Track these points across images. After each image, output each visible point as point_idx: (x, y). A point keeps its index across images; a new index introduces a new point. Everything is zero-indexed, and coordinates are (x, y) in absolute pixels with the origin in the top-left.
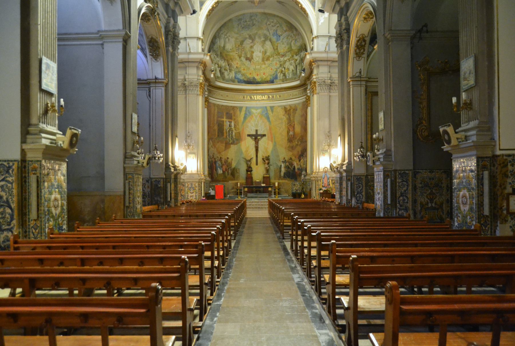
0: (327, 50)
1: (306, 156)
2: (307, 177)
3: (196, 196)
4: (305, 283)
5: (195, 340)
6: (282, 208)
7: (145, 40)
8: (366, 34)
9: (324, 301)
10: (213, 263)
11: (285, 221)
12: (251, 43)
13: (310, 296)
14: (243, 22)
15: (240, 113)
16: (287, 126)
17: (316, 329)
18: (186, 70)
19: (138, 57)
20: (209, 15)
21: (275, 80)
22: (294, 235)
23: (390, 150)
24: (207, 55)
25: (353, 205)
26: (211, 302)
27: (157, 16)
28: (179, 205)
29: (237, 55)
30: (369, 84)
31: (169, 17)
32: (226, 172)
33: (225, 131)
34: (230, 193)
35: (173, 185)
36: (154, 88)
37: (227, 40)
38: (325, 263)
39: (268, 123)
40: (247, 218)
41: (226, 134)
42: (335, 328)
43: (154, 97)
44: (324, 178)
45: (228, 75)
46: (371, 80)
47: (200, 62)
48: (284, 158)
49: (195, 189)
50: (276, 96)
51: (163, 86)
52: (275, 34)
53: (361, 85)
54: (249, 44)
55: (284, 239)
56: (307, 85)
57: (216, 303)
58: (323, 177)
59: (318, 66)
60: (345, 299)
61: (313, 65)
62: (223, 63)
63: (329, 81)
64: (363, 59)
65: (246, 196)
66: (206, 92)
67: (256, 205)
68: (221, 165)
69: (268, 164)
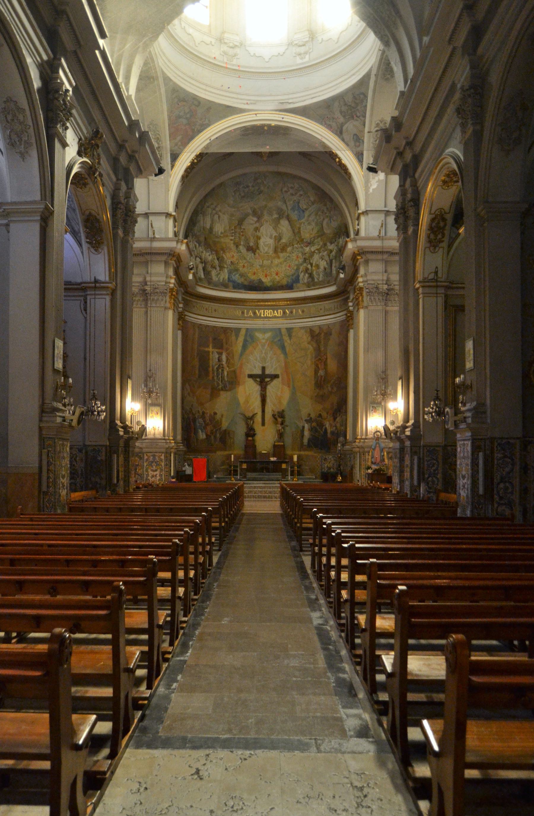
0: (381, 235)
1: (346, 412)
2: (347, 447)
3: (161, 475)
4: (331, 627)
5: (136, 721)
6: (299, 499)
7: (79, 218)
8: (447, 209)
9: (359, 660)
10: (174, 591)
11: (304, 521)
12: (256, 222)
13: (336, 650)
14: (244, 187)
15: (237, 339)
16: (313, 360)
17: (340, 706)
18: (148, 268)
19: (66, 244)
20: (187, 176)
21: (294, 285)
22: (317, 546)
23: (484, 405)
24: (182, 242)
25: (422, 495)
26: (170, 656)
27: (99, 179)
28: (131, 490)
29: (232, 242)
30: (450, 292)
31: (118, 179)
32: (212, 437)
33: (211, 369)
34: (218, 471)
35: (121, 458)
36: (93, 297)
37: (216, 217)
38: (361, 595)
39: (282, 356)
40: (243, 514)
41: (213, 373)
42: (372, 706)
43: (93, 312)
44: (374, 449)
45: (217, 275)
46: (454, 285)
47: (170, 254)
48: (309, 415)
49: (158, 465)
50: (297, 312)
51: (108, 294)
52: (296, 207)
53: (437, 293)
54: (252, 224)
55: (301, 550)
56: (349, 293)
57: (178, 659)
58: (373, 447)
59: (367, 262)
60: (388, 658)
61: (358, 259)
62: (209, 256)
63: (385, 287)
64: (441, 249)
65: (245, 477)
66: (180, 303)
67: (261, 492)
68: (204, 425)
69: (282, 424)
